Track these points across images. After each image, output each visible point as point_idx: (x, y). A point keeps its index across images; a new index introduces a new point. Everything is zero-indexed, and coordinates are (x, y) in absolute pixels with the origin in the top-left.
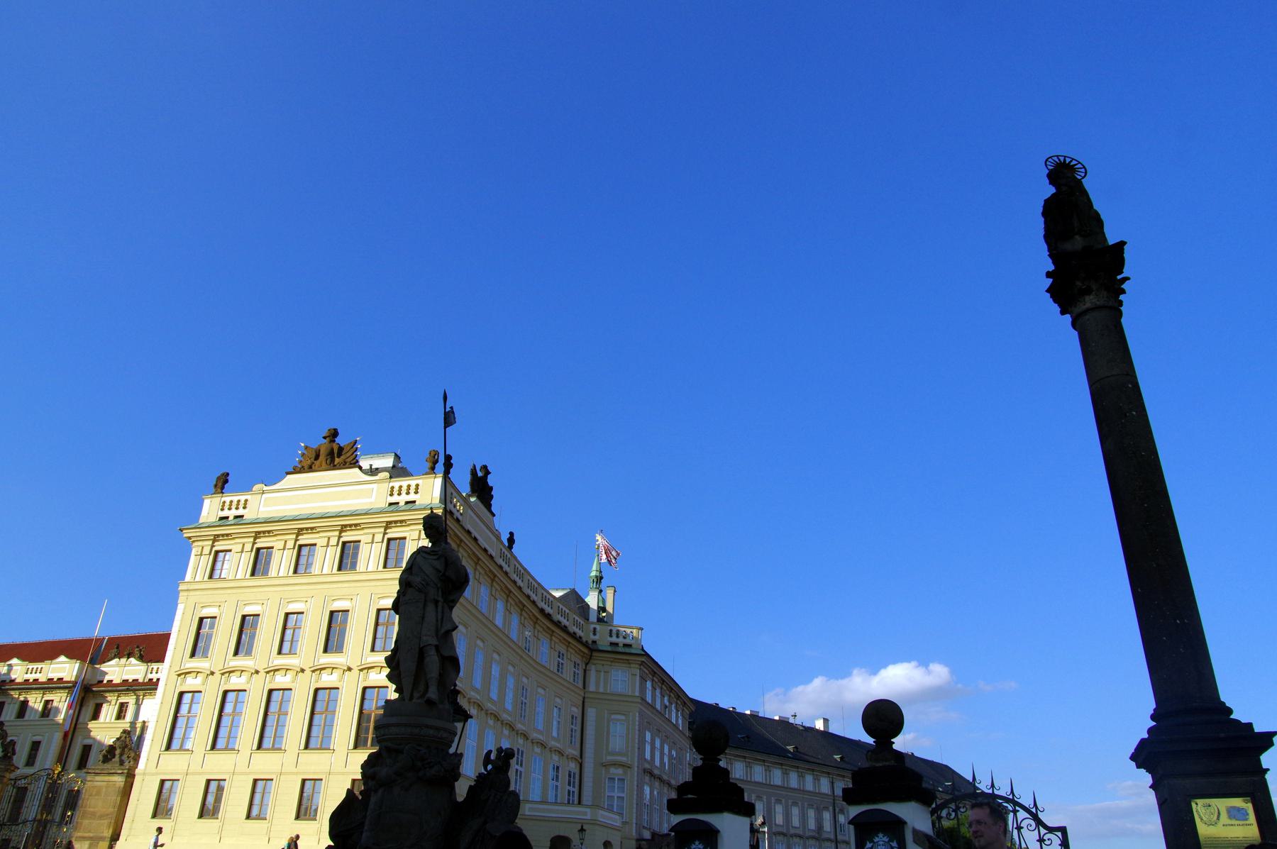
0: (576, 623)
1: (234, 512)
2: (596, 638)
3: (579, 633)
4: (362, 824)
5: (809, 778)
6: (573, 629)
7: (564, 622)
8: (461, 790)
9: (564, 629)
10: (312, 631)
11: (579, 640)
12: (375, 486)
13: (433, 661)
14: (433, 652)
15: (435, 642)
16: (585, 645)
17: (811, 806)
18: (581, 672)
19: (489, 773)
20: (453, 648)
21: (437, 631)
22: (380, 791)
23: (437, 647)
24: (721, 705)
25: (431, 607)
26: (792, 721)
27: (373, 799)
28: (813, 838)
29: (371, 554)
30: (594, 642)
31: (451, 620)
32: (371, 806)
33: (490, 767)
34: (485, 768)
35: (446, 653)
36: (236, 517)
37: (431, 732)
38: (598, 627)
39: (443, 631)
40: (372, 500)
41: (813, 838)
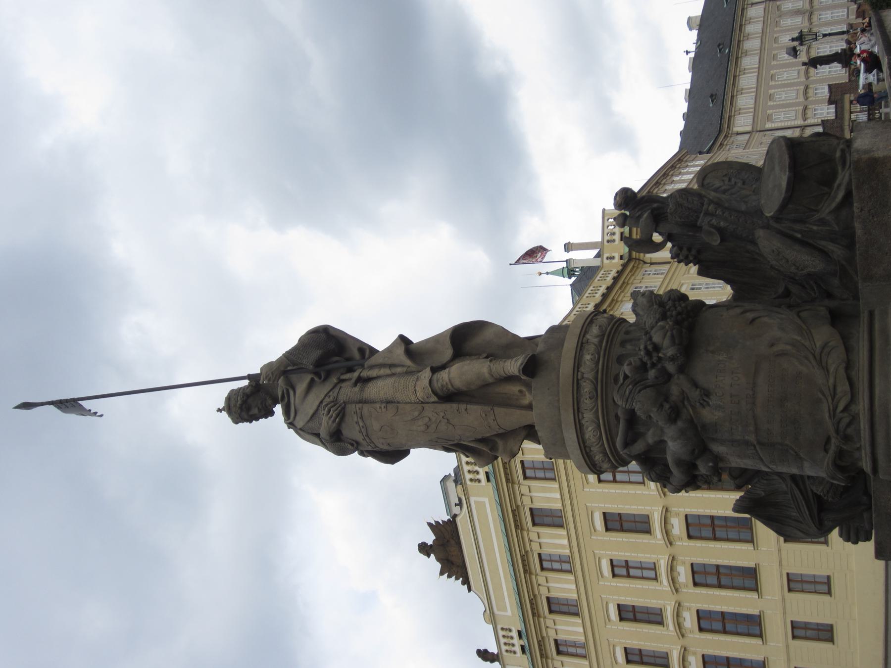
0: (603, 279)
1: (516, 641)
2: (617, 256)
3: (613, 273)
4: (793, 477)
5: (748, 45)
6: (609, 280)
7: (603, 290)
8: (714, 292)
9: (609, 289)
10: (626, 546)
11: (620, 273)
12: (473, 500)
13: (461, 373)
14: (444, 375)
15: (426, 374)
16: (624, 266)
17: (777, 24)
18: (654, 268)
19: (669, 237)
20: (436, 339)
21: (409, 373)
22: (719, 449)
23: (434, 370)
24: (682, 128)
25: (375, 390)
26: (692, 55)
27: (736, 462)
28: (810, 19)
29: (544, 495)
30: (621, 258)
31: (389, 350)
32: (748, 463)
33: (657, 238)
34: (659, 247)
35: (448, 352)
36: (520, 637)
37: (587, 357)
38: (605, 256)
39: (408, 362)
40: (486, 500)
41: (810, 19)
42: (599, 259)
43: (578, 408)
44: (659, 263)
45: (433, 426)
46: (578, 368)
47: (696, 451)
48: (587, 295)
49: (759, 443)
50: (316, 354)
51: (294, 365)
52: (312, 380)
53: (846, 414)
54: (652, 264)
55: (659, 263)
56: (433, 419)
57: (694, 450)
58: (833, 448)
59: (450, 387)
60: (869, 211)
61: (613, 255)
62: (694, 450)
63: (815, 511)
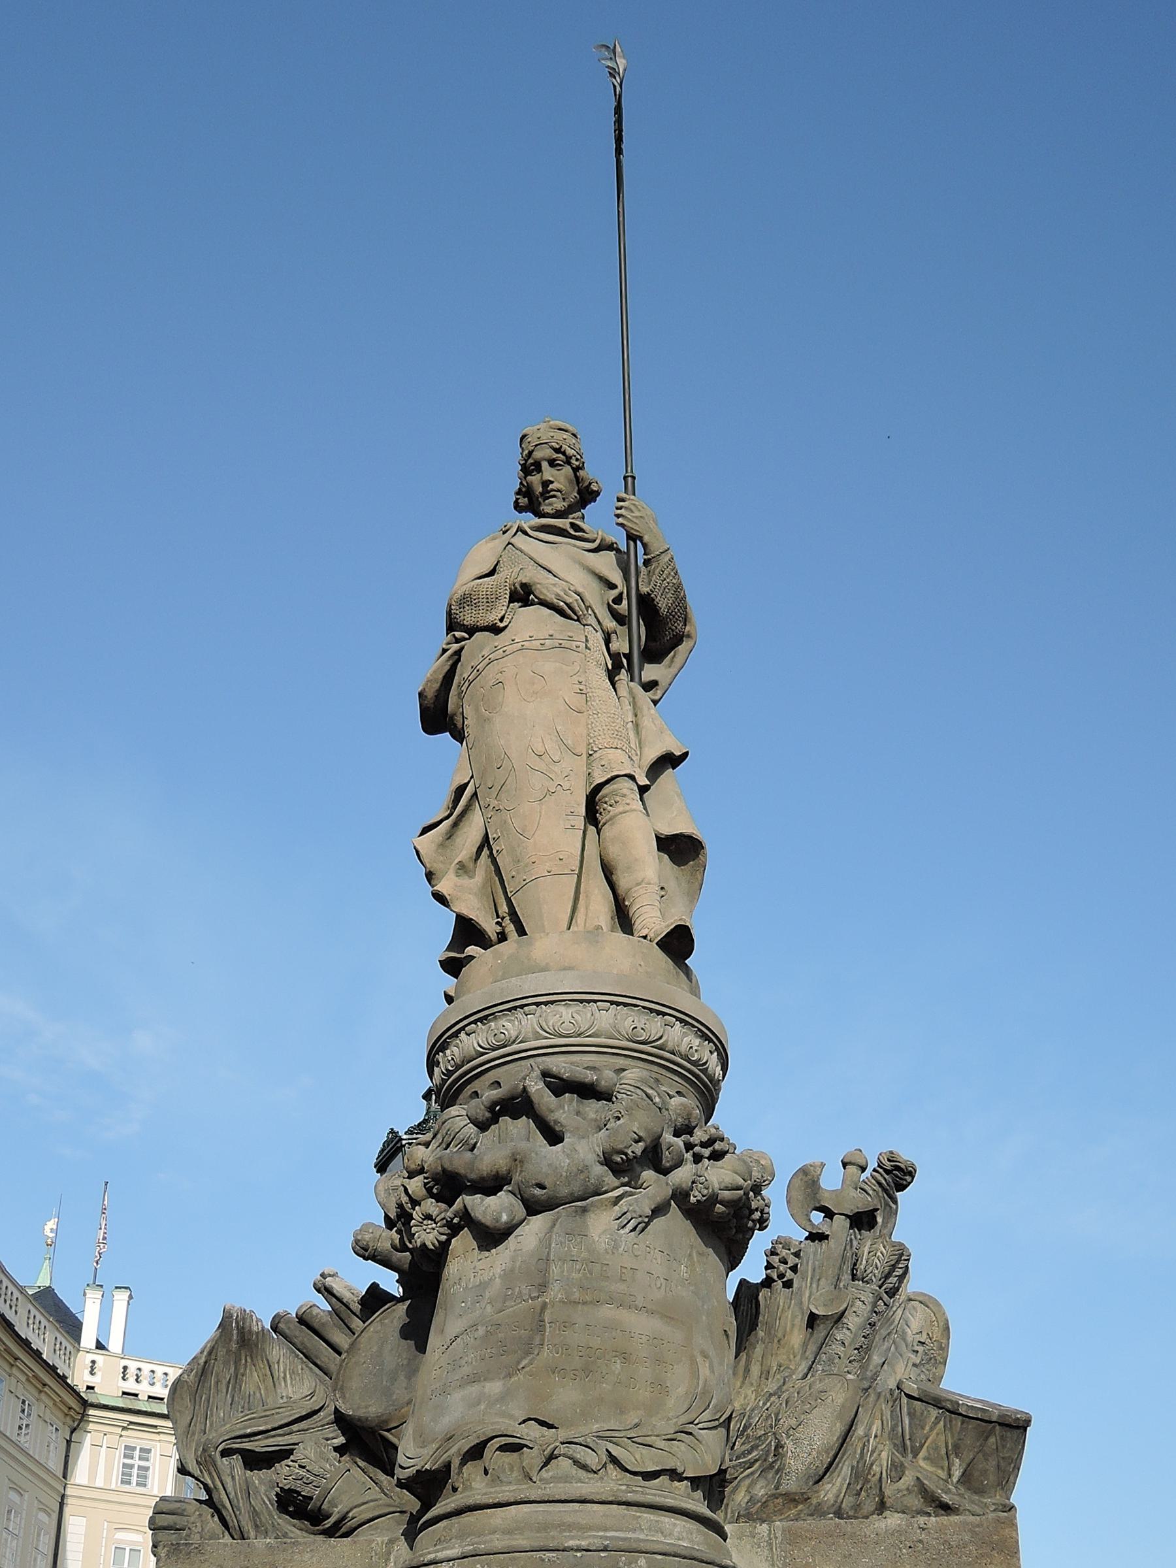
9: (37, 1355)
42: (94, 1347)
43: (618, 1004)
44: (67, 1456)
45: (542, 766)
46: (681, 1021)
47: (538, 1192)
48: (34, 1311)
49: (544, 1306)
50: (663, 604)
51: (647, 563)
52: (613, 586)
53: (604, 1458)
54: (69, 1442)
55: (67, 1456)
56: (556, 768)
57: (542, 1187)
58: (532, 1432)
59: (620, 808)
60: (921, 1541)
61: (99, 1375)
62: (542, 1187)
63: (248, 1446)
